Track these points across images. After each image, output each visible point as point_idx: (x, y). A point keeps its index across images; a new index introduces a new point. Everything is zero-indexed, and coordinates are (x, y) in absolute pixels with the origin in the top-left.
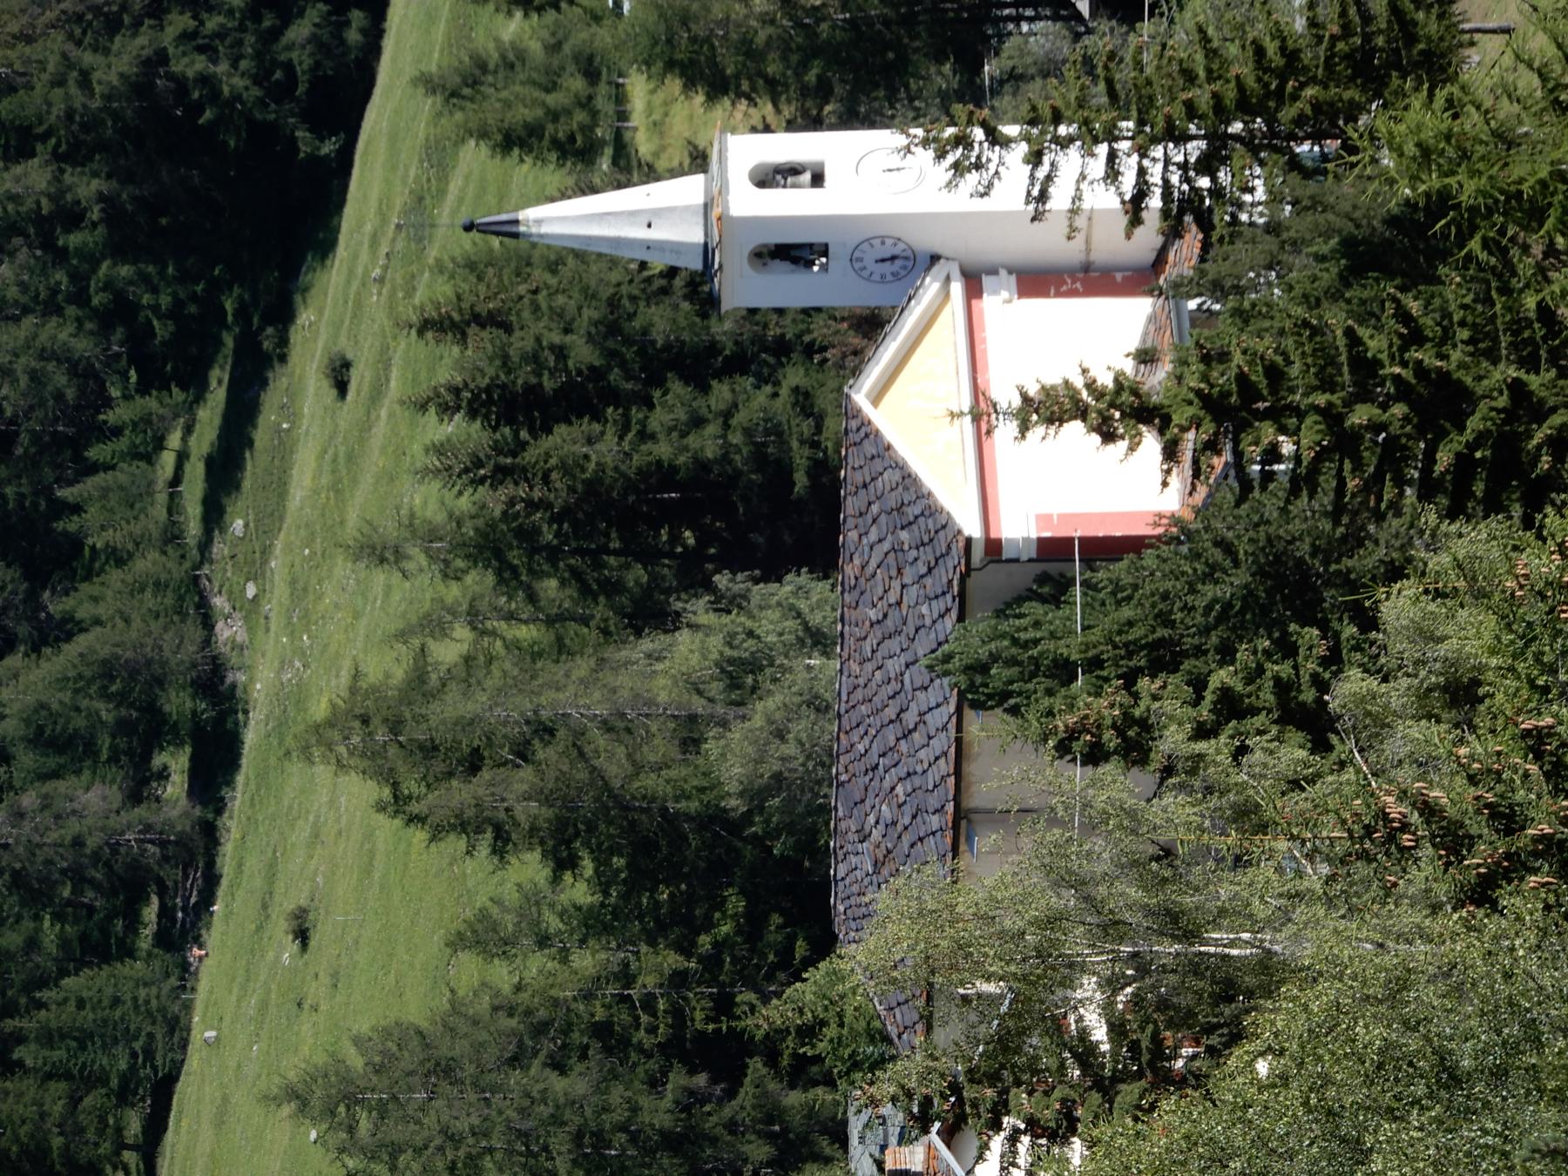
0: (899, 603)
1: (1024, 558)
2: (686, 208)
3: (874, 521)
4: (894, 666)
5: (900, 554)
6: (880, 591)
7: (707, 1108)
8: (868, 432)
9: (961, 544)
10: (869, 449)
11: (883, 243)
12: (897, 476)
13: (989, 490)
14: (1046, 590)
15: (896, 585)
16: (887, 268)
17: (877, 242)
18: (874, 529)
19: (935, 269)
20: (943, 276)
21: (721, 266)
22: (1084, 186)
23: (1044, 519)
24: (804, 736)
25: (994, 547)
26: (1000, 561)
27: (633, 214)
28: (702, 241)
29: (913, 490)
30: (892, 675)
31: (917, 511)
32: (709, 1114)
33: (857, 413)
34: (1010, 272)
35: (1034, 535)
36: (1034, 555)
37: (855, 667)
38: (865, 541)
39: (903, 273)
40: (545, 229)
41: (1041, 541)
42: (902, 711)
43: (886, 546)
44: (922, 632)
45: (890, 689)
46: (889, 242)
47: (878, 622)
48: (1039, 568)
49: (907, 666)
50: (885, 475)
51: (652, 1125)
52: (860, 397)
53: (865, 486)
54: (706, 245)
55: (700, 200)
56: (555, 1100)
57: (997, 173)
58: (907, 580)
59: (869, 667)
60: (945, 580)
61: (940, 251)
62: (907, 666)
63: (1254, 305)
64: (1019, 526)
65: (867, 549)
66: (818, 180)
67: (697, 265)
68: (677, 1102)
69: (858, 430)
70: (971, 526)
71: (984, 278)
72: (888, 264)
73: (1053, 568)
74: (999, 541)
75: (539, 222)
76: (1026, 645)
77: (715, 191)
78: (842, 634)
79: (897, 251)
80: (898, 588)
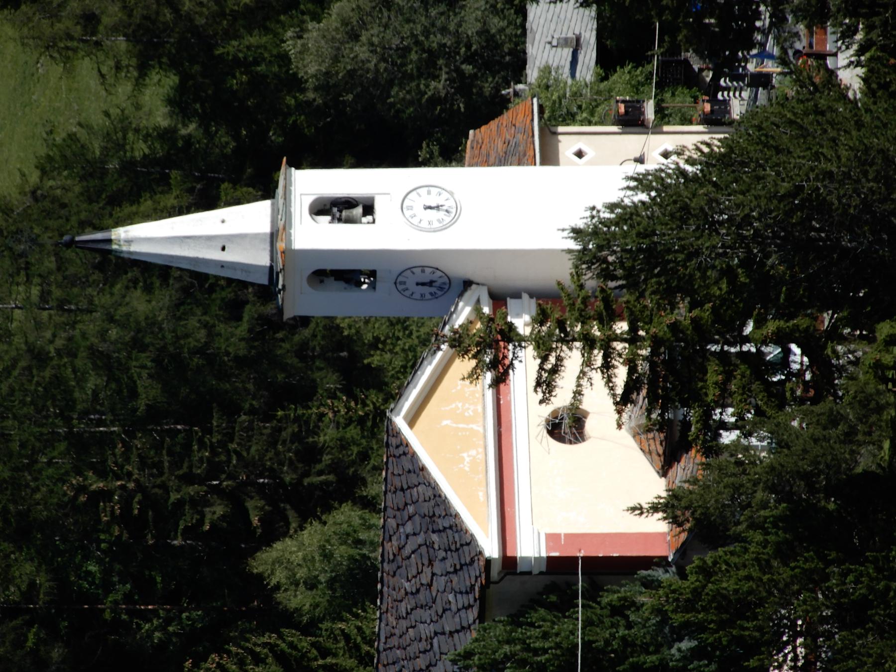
0: (430, 585)
1: (536, 572)
2: (256, 236)
3: (410, 518)
4: (425, 630)
5: (431, 550)
6: (414, 572)
7: (280, 335)
8: (404, 451)
9: (482, 563)
10: (406, 463)
11: (423, 271)
12: (430, 493)
13: (507, 509)
14: (553, 598)
15: (428, 571)
16: (426, 290)
17: (417, 271)
18: (409, 524)
19: (467, 294)
20: (475, 299)
21: (284, 286)
22: (584, 382)
23: (552, 538)
24: (375, 40)
25: (509, 563)
26: (515, 574)
27: (209, 239)
28: (268, 264)
29: (442, 507)
30: (424, 637)
31: (447, 525)
32: (282, 340)
33: (398, 434)
34: (531, 296)
35: (544, 554)
36: (544, 569)
37: (392, 620)
38: (401, 530)
39: (439, 293)
40: (134, 248)
41: (550, 559)
42: (430, 665)
43: (420, 540)
44: (448, 613)
45: (423, 645)
46: (428, 270)
47: (412, 593)
48: (547, 579)
49: (436, 634)
50: (419, 488)
51: (228, 354)
52: (399, 421)
53: (402, 490)
54: (271, 267)
55: (267, 229)
56: (138, 323)
57: (512, 364)
58: (437, 570)
59: (404, 624)
60: (468, 584)
61: (472, 278)
62: (436, 634)
63: (715, 563)
64: (530, 547)
65: (403, 537)
66: (369, 209)
67: (265, 281)
68: (250, 331)
69: (397, 447)
70: (490, 548)
71: (508, 299)
72: (434, 211)
73: (560, 579)
74: (515, 558)
75: (129, 242)
76: (536, 652)
77: (281, 224)
78: (381, 592)
79: (434, 277)
80: (430, 575)
